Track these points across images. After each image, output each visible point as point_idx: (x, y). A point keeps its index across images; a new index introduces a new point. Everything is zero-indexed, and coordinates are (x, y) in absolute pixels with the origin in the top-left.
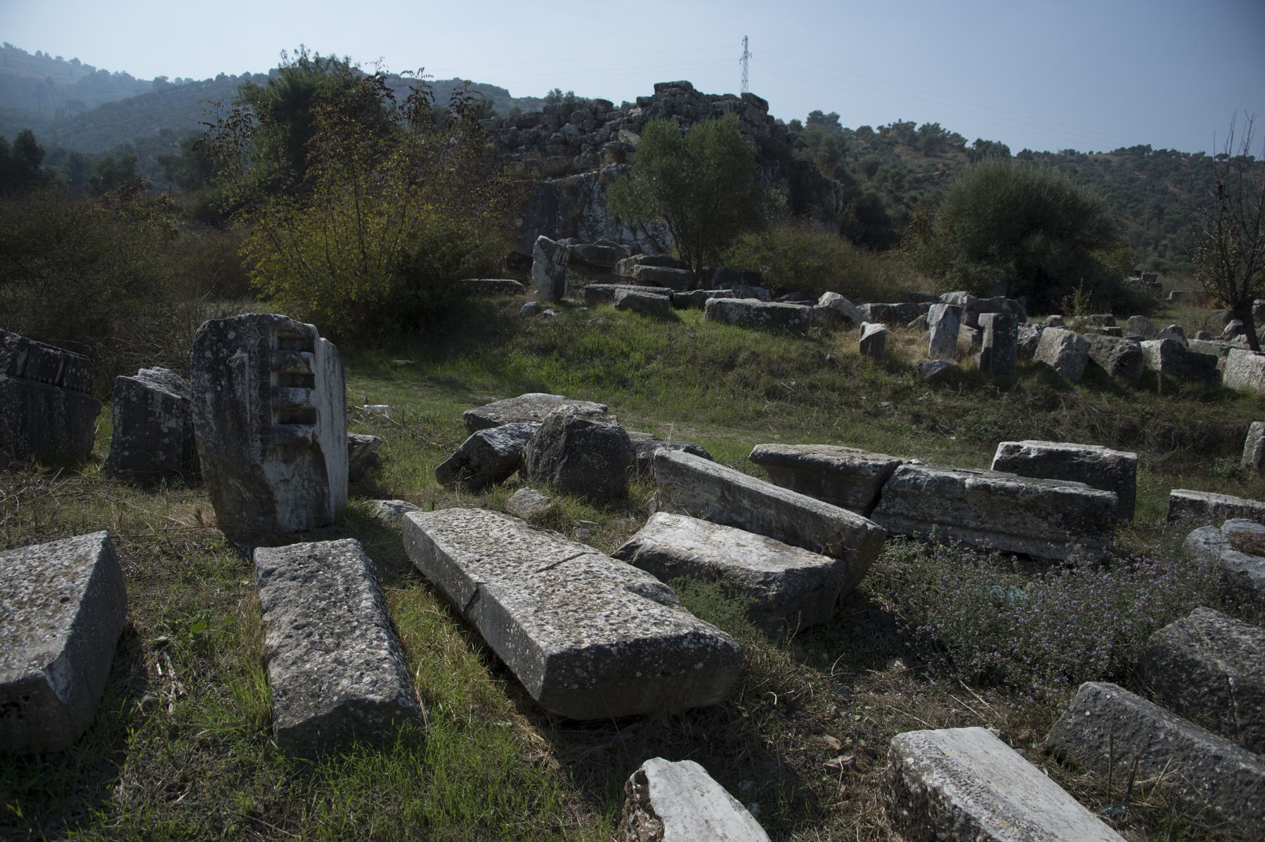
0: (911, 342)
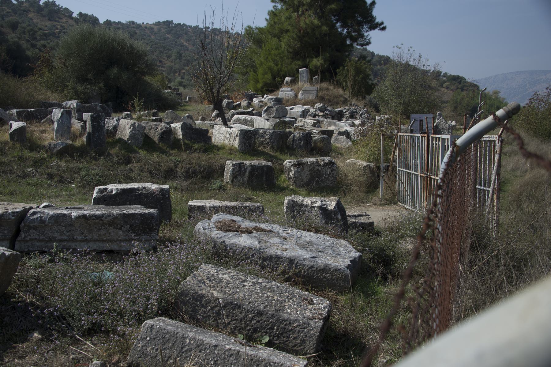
0: (44, 131)
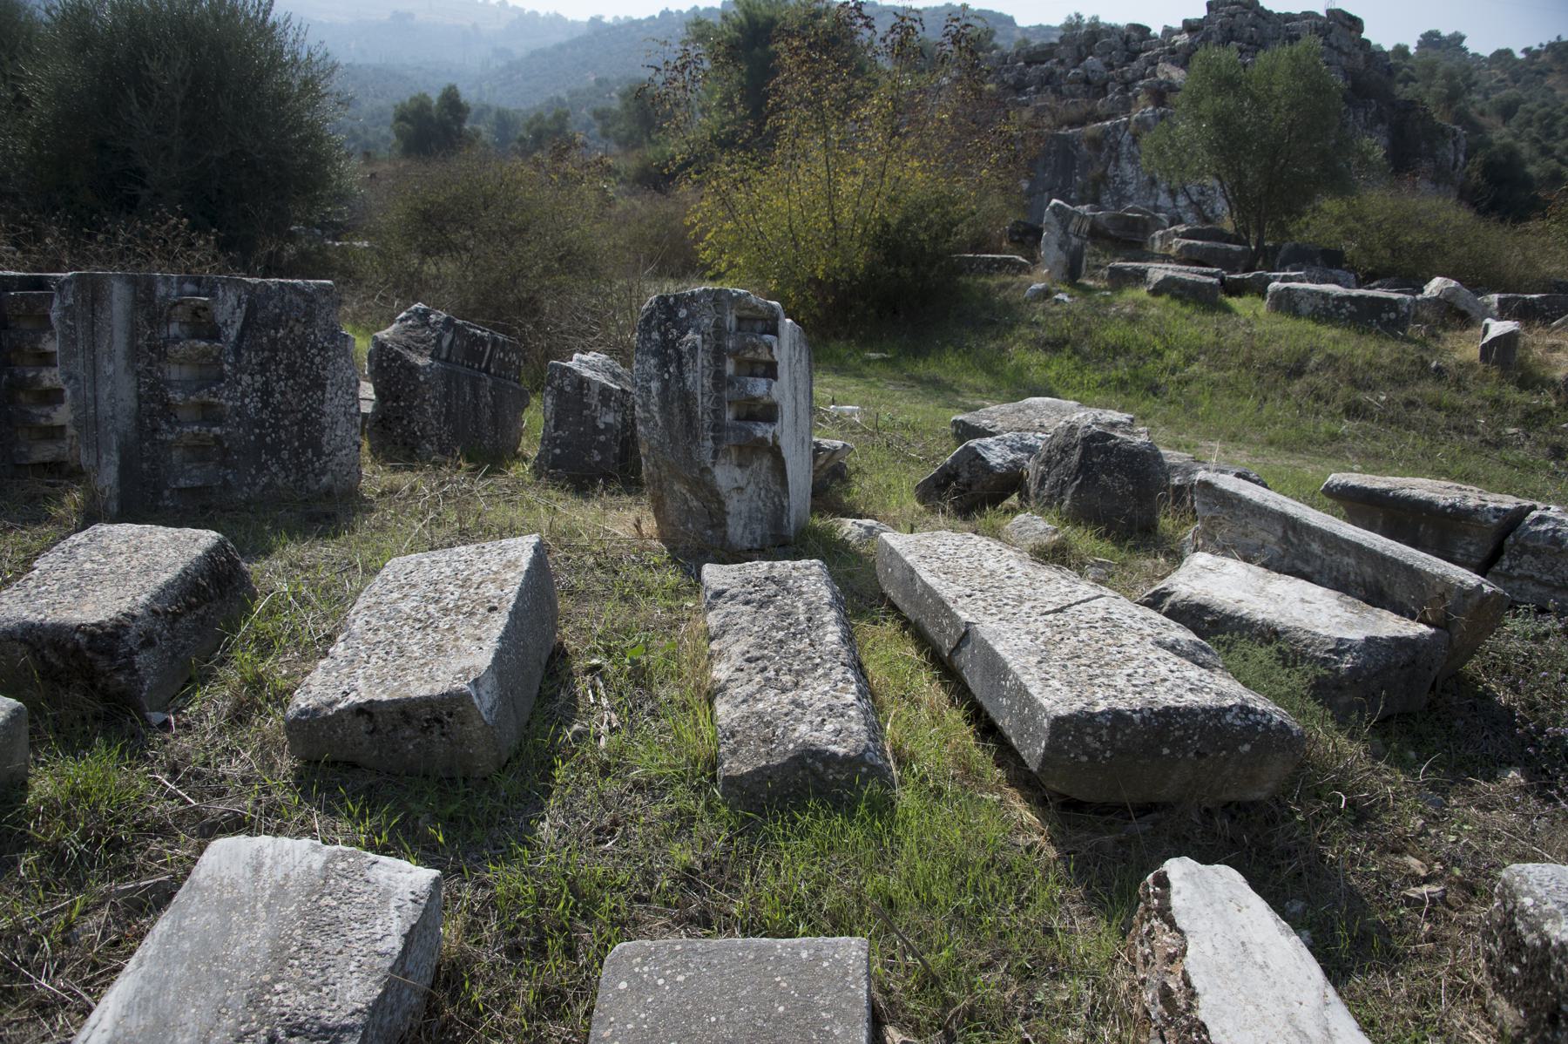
0: (1555, 348)
